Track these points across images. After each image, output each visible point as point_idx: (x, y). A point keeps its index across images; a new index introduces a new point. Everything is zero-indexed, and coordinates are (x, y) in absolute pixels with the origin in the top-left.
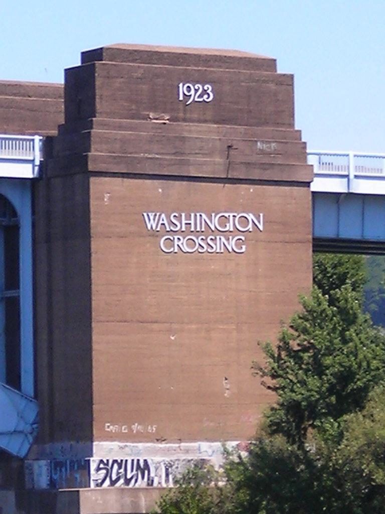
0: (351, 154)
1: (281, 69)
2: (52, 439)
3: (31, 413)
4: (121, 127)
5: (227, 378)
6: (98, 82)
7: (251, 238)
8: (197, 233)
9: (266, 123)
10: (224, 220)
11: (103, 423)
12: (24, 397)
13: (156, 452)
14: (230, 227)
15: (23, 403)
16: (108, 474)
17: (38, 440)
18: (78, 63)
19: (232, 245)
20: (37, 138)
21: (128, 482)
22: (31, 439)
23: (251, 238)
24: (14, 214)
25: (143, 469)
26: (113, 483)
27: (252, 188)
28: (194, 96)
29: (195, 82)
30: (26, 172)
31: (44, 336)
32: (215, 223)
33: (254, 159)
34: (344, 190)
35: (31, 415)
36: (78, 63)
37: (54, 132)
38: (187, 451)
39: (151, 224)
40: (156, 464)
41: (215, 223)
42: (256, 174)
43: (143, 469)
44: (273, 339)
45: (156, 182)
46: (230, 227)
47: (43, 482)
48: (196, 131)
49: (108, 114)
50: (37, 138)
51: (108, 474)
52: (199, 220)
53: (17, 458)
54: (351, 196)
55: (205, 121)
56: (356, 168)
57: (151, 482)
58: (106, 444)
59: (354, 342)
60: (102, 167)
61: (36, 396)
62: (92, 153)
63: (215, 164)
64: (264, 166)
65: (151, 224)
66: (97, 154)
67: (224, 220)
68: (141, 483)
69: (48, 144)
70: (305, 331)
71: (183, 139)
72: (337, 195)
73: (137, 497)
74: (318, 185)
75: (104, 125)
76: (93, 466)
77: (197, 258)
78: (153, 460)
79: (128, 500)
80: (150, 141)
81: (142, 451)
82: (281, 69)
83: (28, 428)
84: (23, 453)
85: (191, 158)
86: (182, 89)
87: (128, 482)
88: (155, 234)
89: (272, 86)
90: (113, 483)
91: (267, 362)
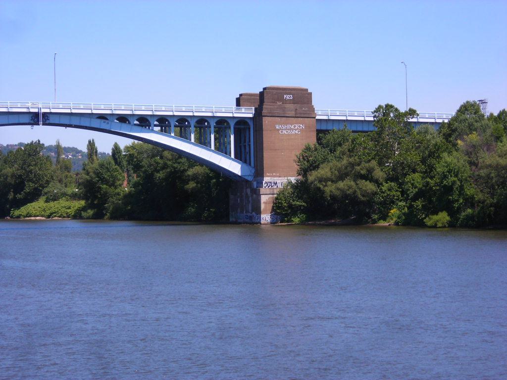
0: (51, 102)
1: (309, 91)
2: (257, 177)
3: (253, 171)
4: (271, 105)
6: (265, 95)
7: (302, 130)
8: (288, 129)
9: (305, 103)
10: (295, 126)
11: (266, 173)
12: (252, 167)
14: (296, 128)
15: (251, 168)
17: (254, 177)
19: (297, 132)
20: (253, 108)
21: (272, 187)
23: (302, 130)
24: (249, 125)
25: (276, 184)
27: (301, 119)
28: (288, 98)
30: (251, 116)
31: (255, 153)
32: (293, 127)
33: (302, 112)
34: (232, 116)
37: (257, 107)
39: (277, 128)
42: (302, 116)
43: (276, 184)
44: (298, 153)
45: (279, 118)
46: (296, 128)
47: (255, 186)
48: (287, 106)
49: (268, 102)
50: (253, 108)
52: (289, 126)
54: (329, 120)
55: (291, 103)
56: (330, 113)
57: (277, 187)
58: (267, 178)
60: (265, 115)
61: (254, 167)
62: (263, 111)
63: (292, 113)
64: (304, 114)
65: (277, 128)
66: (264, 112)
67: (295, 126)
68: (275, 187)
69: (256, 109)
70: (305, 152)
71: (285, 108)
72: (362, 121)
73: (274, 190)
74: (318, 117)
75: (266, 105)
76: (264, 183)
77: (289, 135)
79: (271, 191)
80: (277, 109)
81: (276, 179)
82: (309, 91)
83: (252, 174)
85: (287, 112)
86: (285, 96)
87: (272, 187)
88: (278, 130)
89: (307, 95)
91: (296, 159)
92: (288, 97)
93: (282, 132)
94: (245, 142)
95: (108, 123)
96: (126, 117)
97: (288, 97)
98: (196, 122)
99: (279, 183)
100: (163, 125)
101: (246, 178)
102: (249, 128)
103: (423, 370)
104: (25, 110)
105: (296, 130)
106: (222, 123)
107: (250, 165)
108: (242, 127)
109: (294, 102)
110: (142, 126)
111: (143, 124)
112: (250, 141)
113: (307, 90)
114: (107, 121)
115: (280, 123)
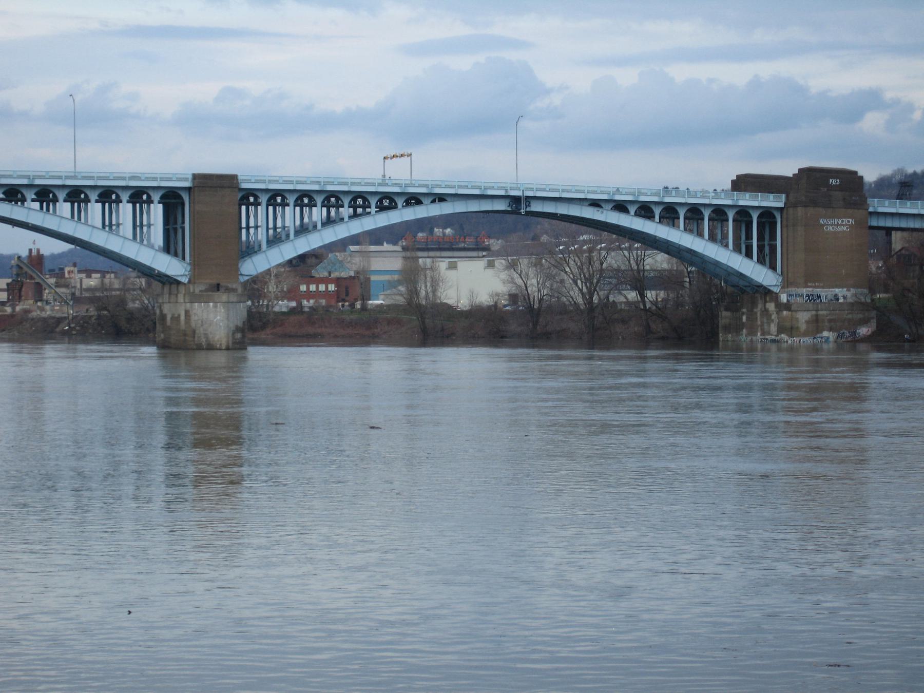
2: (787, 287)
5: (36, 242)
7: (851, 226)
8: (835, 225)
10: (843, 221)
12: (778, 274)
13: (822, 291)
15: (186, 265)
16: (809, 298)
18: (735, 178)
19: (845, 229)
21: (814, 300)
22: (780, 287)
23: (851, 226)
26: (810, 301)
28: (834, 183)
29: (834, 179)
35: (780, 279)
36: (735, 178)
38: (832, 291)
39: (822, 222)
40: (432, 269)
41: (840, 222)
43: (819, 297)
46: (844, 223)
51: (809, 298)
52: (836, 221)
53: (776, 293)
57: (821, 301)
59: (157, 248)
65: (822, 222)
67: (843, 221)
77: (835, 233)
78: (823, 294)
84: (778, 292)
86: (831, 181)
87: (814, 300)
90: (810, 301)
92: (834, 182)
93: (827, 228)
94: (176, 223)
95: (602, 212)
96: (625, 204)
97: (834, 182)
98: (736, 213)
99: (823, 297)
100: (42, 199)
101: (179, 279)
102: (183, 205)
103: (669, 471)
104: (502, 193)
105: (843, 225)
106: (719, 212)
107: (184, 258)
108: (173, 201)
109: (840, 188)
110: (10, 201)
111: (10, 198)
112: (183, 222)
113: (856, 173)
114: (601, 210)
115: (825, 217)
